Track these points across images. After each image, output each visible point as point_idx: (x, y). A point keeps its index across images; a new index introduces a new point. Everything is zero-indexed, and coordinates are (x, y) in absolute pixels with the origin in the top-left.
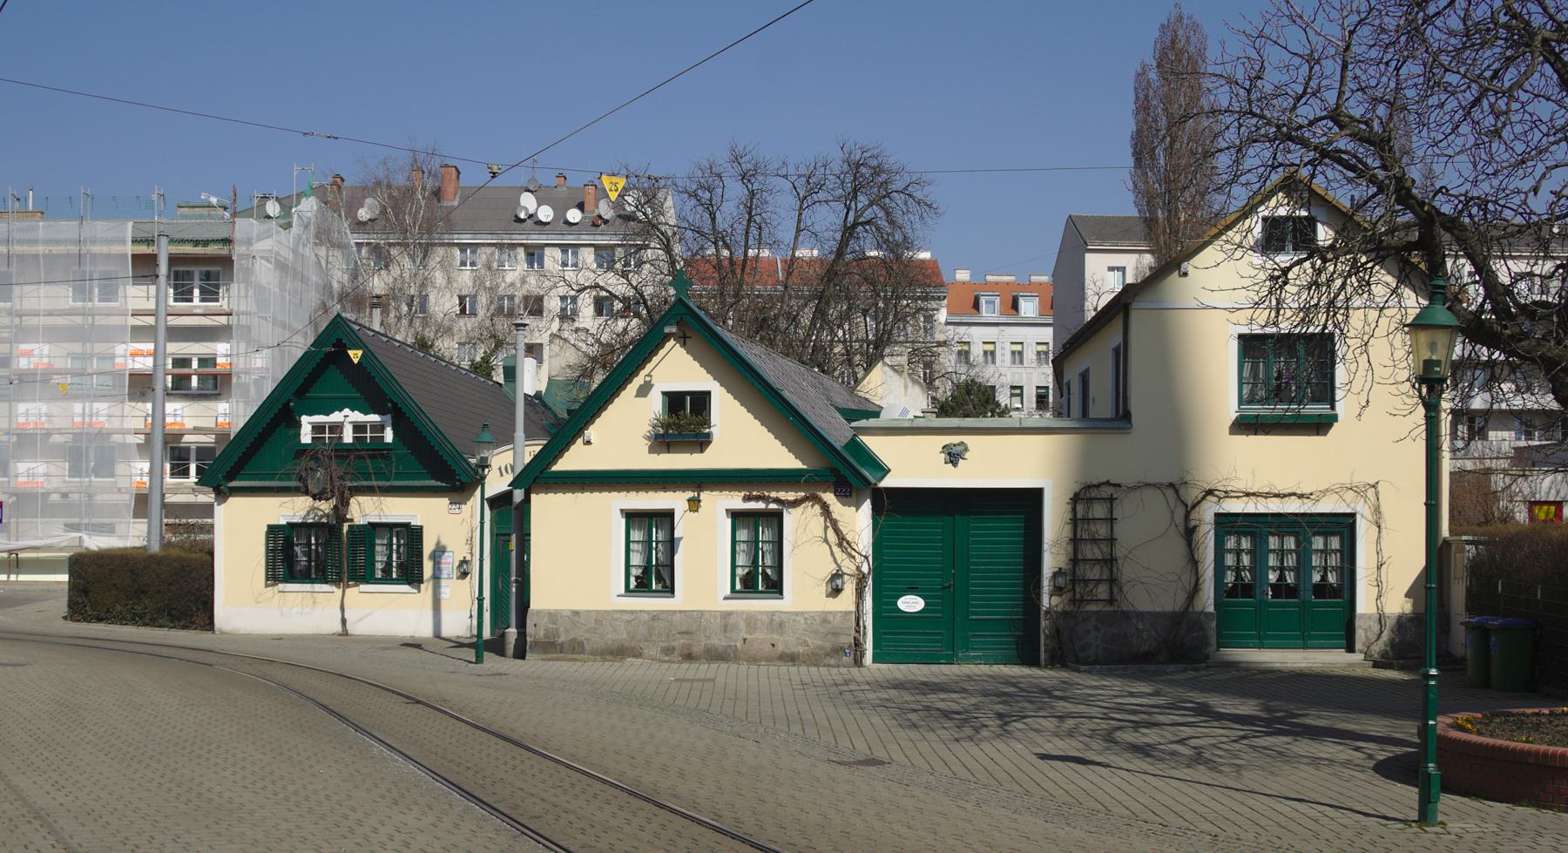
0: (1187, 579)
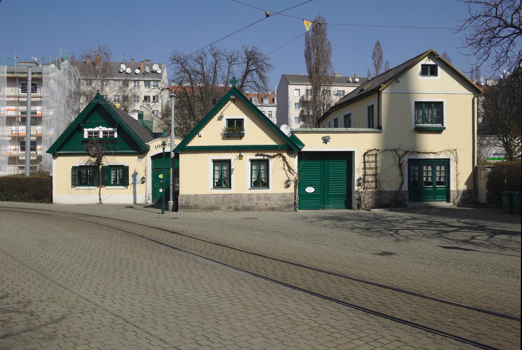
0: (400, 181)
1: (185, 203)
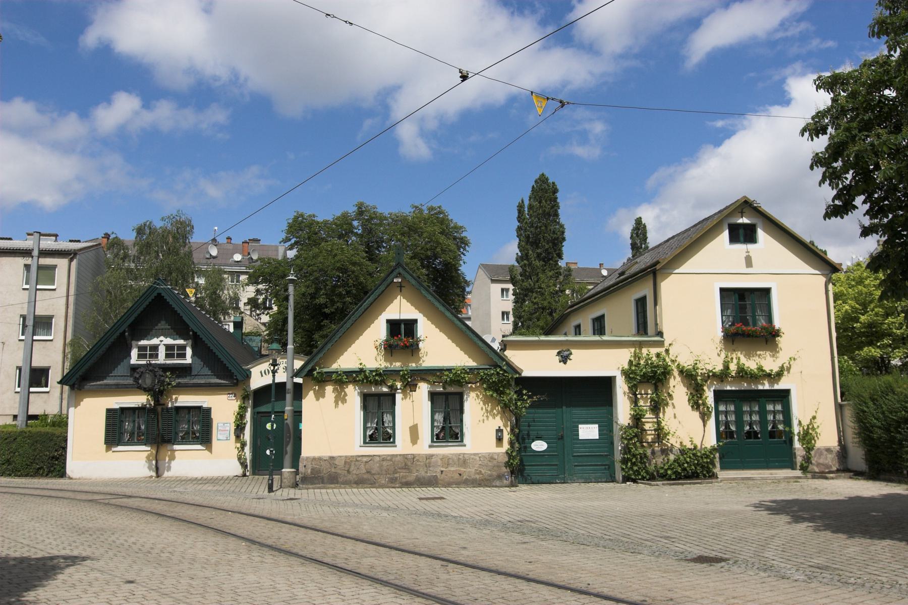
1: (311, 472)
